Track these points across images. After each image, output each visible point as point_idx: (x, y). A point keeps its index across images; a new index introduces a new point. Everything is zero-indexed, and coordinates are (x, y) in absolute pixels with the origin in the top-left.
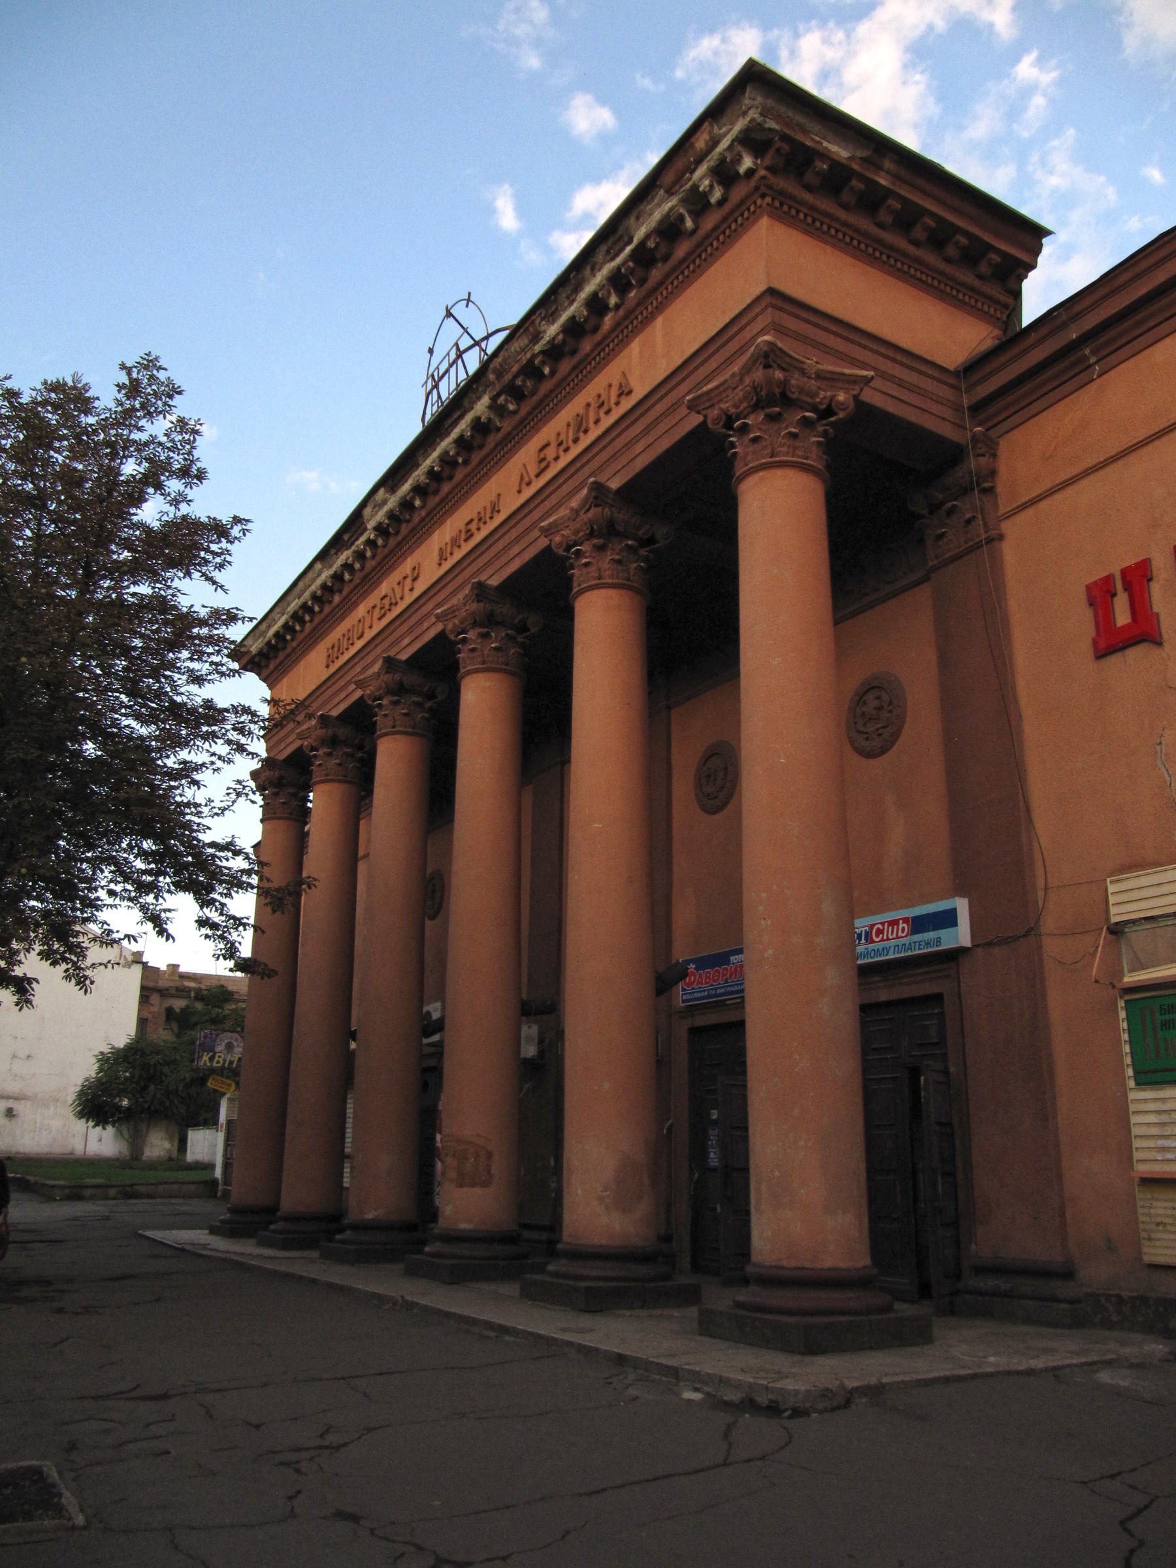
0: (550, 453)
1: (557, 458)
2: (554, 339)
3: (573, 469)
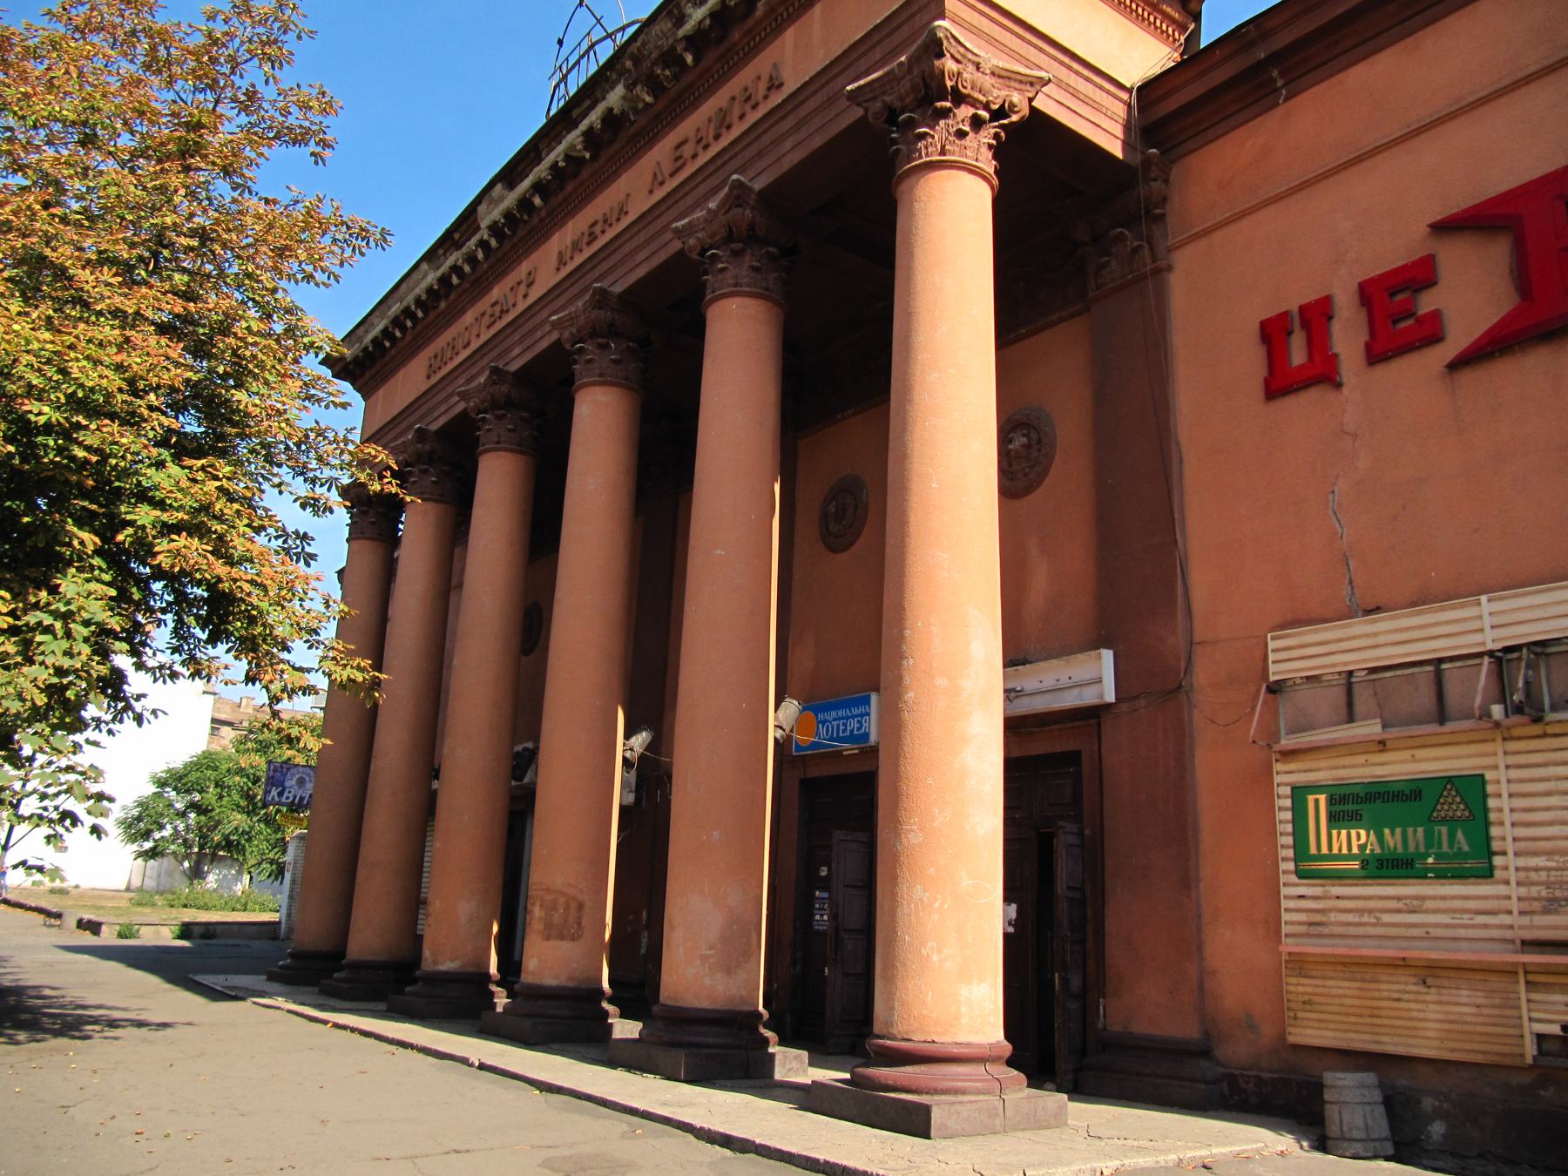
0: (687, 150)
1: (694, 156)
2: (700, 23)
3: (712, 168)
